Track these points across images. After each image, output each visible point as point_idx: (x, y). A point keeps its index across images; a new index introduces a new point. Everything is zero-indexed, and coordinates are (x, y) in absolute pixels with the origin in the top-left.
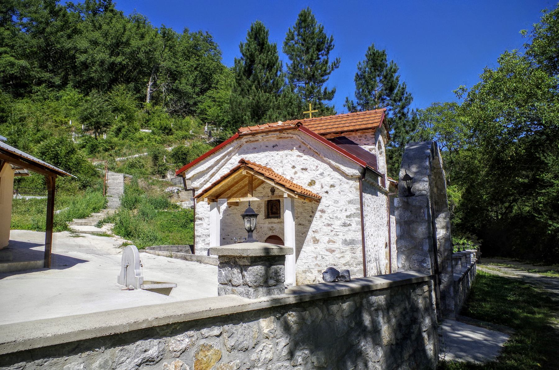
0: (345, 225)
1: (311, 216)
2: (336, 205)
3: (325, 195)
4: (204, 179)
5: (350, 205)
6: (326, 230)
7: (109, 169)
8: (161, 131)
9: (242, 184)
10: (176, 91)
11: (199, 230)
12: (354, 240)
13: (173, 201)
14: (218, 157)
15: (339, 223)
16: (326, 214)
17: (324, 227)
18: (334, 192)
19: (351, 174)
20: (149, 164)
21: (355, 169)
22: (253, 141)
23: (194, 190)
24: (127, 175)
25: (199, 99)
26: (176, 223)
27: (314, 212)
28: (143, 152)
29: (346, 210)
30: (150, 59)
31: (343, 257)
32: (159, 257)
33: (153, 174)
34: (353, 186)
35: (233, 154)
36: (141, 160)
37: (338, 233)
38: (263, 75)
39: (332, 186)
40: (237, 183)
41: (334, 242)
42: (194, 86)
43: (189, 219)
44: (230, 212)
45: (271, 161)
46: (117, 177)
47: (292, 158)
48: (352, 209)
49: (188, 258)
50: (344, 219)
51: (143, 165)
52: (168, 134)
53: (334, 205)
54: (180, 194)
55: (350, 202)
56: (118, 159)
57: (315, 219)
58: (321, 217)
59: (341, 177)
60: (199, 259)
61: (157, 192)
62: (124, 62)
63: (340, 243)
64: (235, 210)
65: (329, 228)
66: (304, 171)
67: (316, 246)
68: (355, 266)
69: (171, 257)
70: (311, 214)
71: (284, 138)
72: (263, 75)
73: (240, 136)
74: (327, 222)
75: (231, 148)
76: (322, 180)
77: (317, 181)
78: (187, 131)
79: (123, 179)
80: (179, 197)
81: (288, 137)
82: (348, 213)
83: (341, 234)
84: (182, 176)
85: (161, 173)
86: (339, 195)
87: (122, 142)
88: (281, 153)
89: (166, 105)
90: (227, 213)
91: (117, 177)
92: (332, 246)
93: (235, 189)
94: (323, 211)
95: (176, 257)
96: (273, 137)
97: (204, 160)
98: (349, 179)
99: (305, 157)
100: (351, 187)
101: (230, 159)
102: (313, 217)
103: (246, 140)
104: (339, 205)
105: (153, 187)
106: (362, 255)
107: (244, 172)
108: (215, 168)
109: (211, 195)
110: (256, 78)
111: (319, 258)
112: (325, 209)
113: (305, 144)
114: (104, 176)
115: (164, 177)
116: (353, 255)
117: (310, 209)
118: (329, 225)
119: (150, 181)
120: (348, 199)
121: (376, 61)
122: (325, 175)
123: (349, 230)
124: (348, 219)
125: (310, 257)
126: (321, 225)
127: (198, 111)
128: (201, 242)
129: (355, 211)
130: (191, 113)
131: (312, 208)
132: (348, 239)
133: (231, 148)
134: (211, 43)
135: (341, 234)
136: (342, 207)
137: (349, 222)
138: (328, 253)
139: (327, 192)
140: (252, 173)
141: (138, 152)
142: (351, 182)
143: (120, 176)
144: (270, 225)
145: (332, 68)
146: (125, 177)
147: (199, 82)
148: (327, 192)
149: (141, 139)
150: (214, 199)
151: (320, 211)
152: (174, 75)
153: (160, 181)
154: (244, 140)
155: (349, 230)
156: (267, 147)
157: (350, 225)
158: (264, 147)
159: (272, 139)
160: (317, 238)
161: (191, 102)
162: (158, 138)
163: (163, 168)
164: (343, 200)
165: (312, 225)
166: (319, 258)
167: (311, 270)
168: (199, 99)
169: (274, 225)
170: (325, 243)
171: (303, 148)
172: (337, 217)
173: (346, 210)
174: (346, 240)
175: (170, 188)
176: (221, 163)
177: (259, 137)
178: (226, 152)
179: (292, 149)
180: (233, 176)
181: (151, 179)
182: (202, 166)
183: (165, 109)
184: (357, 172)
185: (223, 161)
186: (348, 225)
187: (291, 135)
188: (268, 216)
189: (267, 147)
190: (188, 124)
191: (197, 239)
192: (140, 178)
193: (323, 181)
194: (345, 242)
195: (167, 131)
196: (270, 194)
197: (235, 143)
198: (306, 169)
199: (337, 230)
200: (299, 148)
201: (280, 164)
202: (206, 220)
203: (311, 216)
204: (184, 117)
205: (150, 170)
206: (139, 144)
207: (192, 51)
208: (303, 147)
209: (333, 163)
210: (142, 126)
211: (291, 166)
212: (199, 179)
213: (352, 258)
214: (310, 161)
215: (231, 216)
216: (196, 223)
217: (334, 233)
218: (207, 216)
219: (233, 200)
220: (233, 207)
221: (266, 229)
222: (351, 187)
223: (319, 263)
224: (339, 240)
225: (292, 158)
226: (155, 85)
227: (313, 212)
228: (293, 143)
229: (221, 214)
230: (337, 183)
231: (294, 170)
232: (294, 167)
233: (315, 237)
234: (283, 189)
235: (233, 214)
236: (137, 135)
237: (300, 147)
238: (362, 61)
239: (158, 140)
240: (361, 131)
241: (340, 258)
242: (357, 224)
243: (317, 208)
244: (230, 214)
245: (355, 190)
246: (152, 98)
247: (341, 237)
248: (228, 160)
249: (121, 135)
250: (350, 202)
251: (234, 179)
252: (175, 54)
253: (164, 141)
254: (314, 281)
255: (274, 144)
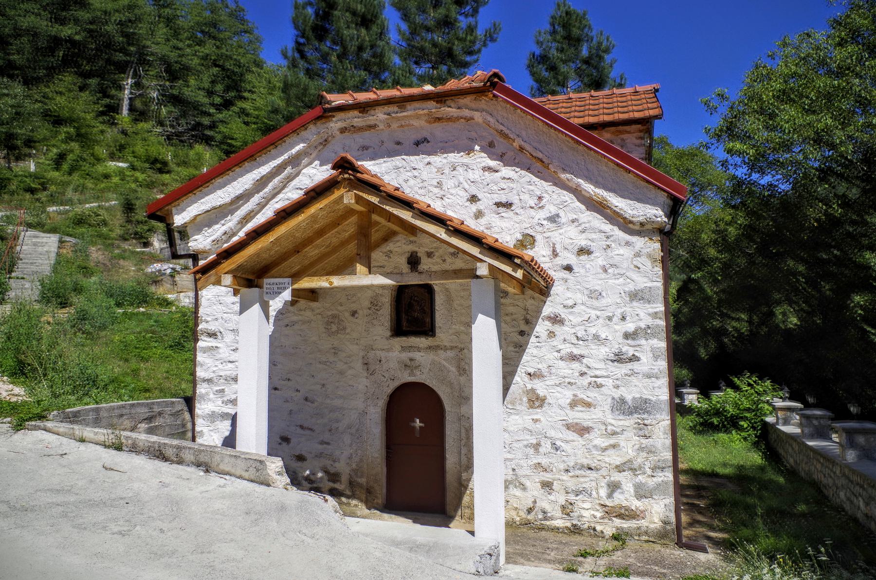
0: (619, 358)
1: (522, 333)
2: (595, 303)
3: (565, 274)
4: (224, 228)
5: (635, 304)
6: (568, 372)
7: (30, 226)
8: (147, 165)
9: (332, 238)
10: (176, 100)
11: (207, 365)
12: (646, 401)
13: (159, 291)
14: (264, 170)
15: (604, 351)
16: (565, 328)
17: (562, 364)
18: (588, 270)
19: (641, 219)
20: (117, 221)
21: (653, 204)
22: (360, 129)
23: (195, 257)
24: (68, 239)
25: (220, 116)
26: (160, 340)
27: (530, 322)
28: (108, 201)
29: (623, 318)
30: (130, 38)
31: (614, 446)
32: (83, 447)
33: (124, 239)
34: (645, 251)
35: (305, 161)
36: (101, 212)
37: (599, 380)
38: (351, 33)
39: (583, 251)
40: (321, 233)
41: (589, 405)
42: (210, 93)
43: (186, 332)
44: (295, 318)
45: (412, 182)
46: (45, 240)
47: (471, 175)
48: (642, 315)
49: (170, 452)
50: (617, 343)
51: (104, 221)
52: (161, 171)
53: (590, 302)
54: (177, 278)
55: (635, 296)
56: (52, 209)
57: (533, 339)
58: (552, 334)
59: (608, 227)
60: (203, 458)
61: (128, 273)
62: (77, 37)
63: (607, 408)
64: (308, 313)
65: (576, 365)
66: (501, 209)
67: (538, 414)
68: (649, 472)
69: (119, 448)
70: (523, 327)
71: (450, 119)
72: (351, 33)
73: (328, 113)
74: (567, 349)
75: (301, 146)
76: (556, 234)
77: (539, 238)
78: (196, 168)
79: (56, 245)
80: (174, 283)
81: (458, 118)
82: (630, 327)
83: (609, 382)
84: (161, 219)
85: (142, 237)
86: (603, 276)
87: (66, 178)
88: (438, 160)
89: (161, 123)
90: (286, 321)
91: (45, 240)
92: (580, 415)
93: (312, 252)
94: (556, 320)
95: (135, 449)
96: (418, 117)
97: (226, 178)
98: (632, 232)
99: (507, 171)
100: (638, 255)
101: (298, 174)
102: (529, 335)
103: (340, 125)
104: (604, 302)
105: (121, 262)
106: (668, 442)
107: (348, 197)
108: (256, 199)
109: (240, 268)
110: (340, 41)
111: (546, 447)
112: (563, 313)
113: (506, 136)
114: (16, 238)
115: (146, 244)
116: (644, 441)
117: (519, 314)
118: (573, 358)
119: (117, 251)
120: (631, 287)
121: (568, 30)
122: (563, 220)
123: (633, 373)
124: (630, 342)
125: (521, 445)
126: (551, 357)
127: (218, 137)
128: (212, 396)
129: (649, 321)
130: (208, 141)
131: (526, 310)
132: (629, 398)
133: (301, 146)
134: (242, 21)
135: (609, 382)
136: (611, 309)
137: (631, 352)
138: (571, 435)
139: (569, 268)
140: (375, 200)
141: (97, 198)
142: (639, 242)
143: (52, 240)
144: (405, 356)
145: (485, 42)
146: (61, 242)
147: (219, 88)
148: (569, 268)
149: (107, 176)
150: (251, 280)
151: (549, 318)
152: (174, 72)
153: (138, 253)
154: (335, 124)
155: (633, 373)
156: (398, 143)
157: (634, 359)
158: (390, 145)
159: (416, 123)
160: (541, 392)
161: (206, 121)
162: (140, 176)
163: (146, 228)
164: (614, 290)
165: (525, 358)
166: (546, 447)
167: (523, 480)
168: (220, 116)
169: (417, 355)
170: (561, 408)
171: (499, 149)
172: (596, 337)
173: (623, 318)
174: (623, 401)
175: (157, 266)
176: (270, 186)
177: (379, 115)
178: (285, 156)
179: (469, 150)
180: (313, 209)
181: (118, 247)
182: (220, 193)
183: (159, 130)
184: (660, 212)
185: (276, 180)
186: (630, 360)
187: (466, 113)
188: (398, 331)
189: (398, 143)
190: (199, 157)
191: (201, 389)
192: (94, 244)
193: (557, 237)
194: (621, 406)
195: (160, 166)
196: (405, 268)
197: (313, 133)
198: (508, 205)
199: (598, 373)
200: (490, 148)
201: (436, 190)
202: (229, 337)
203: (522, 333)
204: (191, 147)
205: (118, 231)
206: (103, 185)
207: (209, 30)
208: (501, 145)
209: (589, 188)
210: (112, 157)
211: (466, 196)
212: (209, 226)
213: (641, 449)
214: (520, 183)
215: (296, 327)
216: (200, 344)
217: (587, 380)
218: (231, 326)
219: (306, 283)
220: (302, 303)
221: (393, 365)
222: (638, 255)
223: (544, 461)
224: (603, 399)
225: (471, 175)
226: (138, 85)
227: (527, 322)
228: (473, 134)
229: (271, 324)
230: (597, 243)
231: (474, 208)
232: (473, 199)
233: (533, 390)
234: (475, 251)
235: (304, 322)
236: (100, 169)
237: (491, 145)
238: (543, 31)
239: (140, 180)
240: (613, 129)
241: (605, 450)
242: (656, 358)
243: (539, 311)
244: (294, 323)
245: (649, 263)
246: (132, 109)
247: (610, 391)
248: (290, 179)
249: (65, 167)
250: (635, 296)
251: (314, 218)
252: (176, 34)
253: (153, 183)
254: (530, 511)
255: (419, 137)
